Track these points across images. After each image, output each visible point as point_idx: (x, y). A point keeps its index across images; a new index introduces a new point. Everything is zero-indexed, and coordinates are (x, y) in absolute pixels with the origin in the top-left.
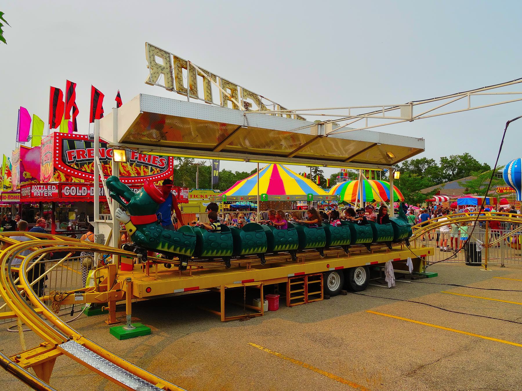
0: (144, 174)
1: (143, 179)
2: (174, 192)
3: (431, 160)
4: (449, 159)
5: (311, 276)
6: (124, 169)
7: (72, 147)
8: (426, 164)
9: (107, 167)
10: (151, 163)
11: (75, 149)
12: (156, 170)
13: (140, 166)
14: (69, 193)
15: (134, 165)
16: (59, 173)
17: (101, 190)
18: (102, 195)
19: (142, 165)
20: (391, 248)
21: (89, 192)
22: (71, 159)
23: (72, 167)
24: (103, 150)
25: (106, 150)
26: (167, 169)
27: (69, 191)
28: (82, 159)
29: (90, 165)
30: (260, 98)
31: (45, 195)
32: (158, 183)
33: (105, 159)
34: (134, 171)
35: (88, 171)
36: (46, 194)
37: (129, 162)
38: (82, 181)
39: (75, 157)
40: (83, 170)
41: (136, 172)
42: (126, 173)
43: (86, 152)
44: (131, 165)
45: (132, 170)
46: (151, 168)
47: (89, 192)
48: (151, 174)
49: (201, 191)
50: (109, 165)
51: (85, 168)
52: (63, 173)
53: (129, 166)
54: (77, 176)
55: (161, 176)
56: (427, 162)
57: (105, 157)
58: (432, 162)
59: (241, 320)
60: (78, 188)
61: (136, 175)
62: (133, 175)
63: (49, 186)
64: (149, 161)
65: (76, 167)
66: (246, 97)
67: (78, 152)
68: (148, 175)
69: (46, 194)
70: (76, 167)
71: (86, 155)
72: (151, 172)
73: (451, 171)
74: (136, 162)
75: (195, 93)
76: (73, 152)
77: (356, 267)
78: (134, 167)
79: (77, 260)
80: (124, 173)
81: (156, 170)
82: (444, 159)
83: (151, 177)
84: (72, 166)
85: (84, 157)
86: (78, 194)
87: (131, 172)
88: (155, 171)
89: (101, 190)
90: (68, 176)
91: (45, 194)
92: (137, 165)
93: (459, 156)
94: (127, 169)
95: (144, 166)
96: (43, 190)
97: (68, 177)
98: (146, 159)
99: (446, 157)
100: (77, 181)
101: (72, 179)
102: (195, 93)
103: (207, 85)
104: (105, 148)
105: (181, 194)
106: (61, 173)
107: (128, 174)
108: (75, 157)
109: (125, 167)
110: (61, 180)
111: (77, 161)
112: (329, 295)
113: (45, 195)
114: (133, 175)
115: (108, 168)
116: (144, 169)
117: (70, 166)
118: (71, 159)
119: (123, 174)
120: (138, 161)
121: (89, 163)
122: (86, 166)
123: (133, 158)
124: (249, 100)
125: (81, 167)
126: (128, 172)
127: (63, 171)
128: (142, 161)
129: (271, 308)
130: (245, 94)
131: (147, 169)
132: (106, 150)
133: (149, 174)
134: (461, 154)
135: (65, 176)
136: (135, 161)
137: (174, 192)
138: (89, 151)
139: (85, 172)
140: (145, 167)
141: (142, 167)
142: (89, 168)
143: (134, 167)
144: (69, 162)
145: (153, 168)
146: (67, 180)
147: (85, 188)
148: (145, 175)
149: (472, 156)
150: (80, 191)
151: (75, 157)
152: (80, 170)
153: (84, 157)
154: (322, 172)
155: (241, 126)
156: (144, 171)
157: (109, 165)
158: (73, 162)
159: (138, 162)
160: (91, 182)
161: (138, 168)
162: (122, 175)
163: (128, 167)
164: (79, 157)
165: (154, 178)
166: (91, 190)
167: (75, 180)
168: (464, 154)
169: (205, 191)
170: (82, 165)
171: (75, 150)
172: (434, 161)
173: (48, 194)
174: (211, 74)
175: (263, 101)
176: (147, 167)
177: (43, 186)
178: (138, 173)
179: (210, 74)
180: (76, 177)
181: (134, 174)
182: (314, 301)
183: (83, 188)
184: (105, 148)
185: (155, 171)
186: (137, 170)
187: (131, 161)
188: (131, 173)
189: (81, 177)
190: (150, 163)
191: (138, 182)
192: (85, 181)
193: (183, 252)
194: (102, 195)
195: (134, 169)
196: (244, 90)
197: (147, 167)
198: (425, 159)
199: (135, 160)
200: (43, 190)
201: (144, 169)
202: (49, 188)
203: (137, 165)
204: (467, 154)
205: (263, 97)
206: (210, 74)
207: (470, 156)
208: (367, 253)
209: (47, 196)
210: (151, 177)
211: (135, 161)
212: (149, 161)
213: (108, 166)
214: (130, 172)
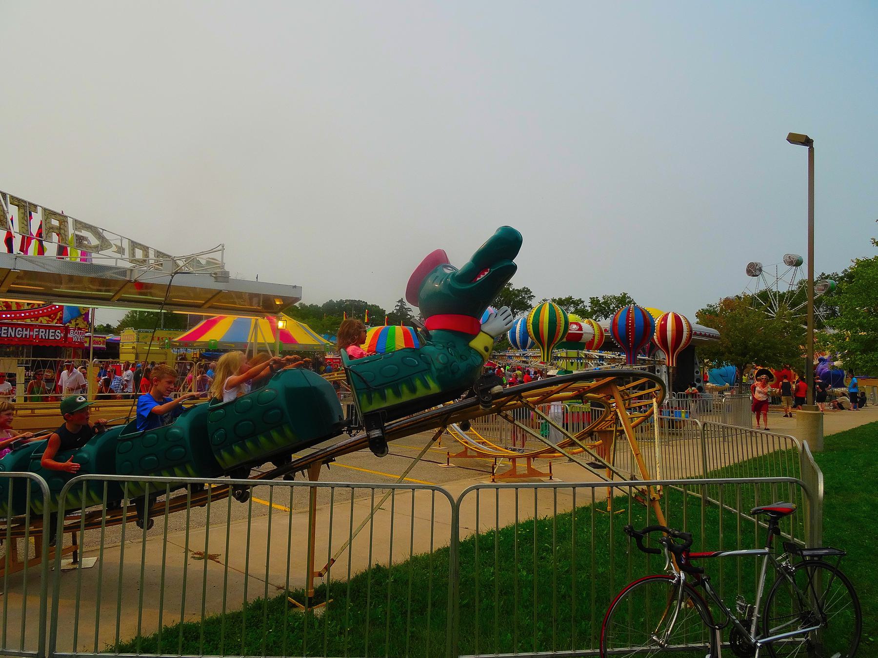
2: (58, 332)
3: (578, 301)
4: (602, 301)
8: (572, 305)
14: (21, 335)
17: (46, 333)
18: (47, 338)
30: (101, 231)
32: (39, 320)
49: (170, 332)
55: (47, 310)
56: (573, 302)
58: (580, 303)
61: (5, 309)
68: (22, 308)
73: (603, 318)
75: (5, 224)
82: (594, 300)
89: (46, 333)
93: (615, 298)
99: (597, 298)
102: (5, 224)
103: (23, 215)
105: (69, 336)
124: (84, 233)
130: (79, 226)
134: (618, 295)
149: (632, 298)
154: (411, 311)
155: (11, 269)
165: (45, 311)
168: (621, 294)
169: (176, 332)
172: (583, 302)
174: (29, 203)
175: (105, 234)
179: (27, 204)
191: (6, 318)
194: (47, 338)
196: (76, 222)
198: (571, 298)
204: (625, 294)
206: (27, 204)
207: (629, 297)
210: (27, 312)
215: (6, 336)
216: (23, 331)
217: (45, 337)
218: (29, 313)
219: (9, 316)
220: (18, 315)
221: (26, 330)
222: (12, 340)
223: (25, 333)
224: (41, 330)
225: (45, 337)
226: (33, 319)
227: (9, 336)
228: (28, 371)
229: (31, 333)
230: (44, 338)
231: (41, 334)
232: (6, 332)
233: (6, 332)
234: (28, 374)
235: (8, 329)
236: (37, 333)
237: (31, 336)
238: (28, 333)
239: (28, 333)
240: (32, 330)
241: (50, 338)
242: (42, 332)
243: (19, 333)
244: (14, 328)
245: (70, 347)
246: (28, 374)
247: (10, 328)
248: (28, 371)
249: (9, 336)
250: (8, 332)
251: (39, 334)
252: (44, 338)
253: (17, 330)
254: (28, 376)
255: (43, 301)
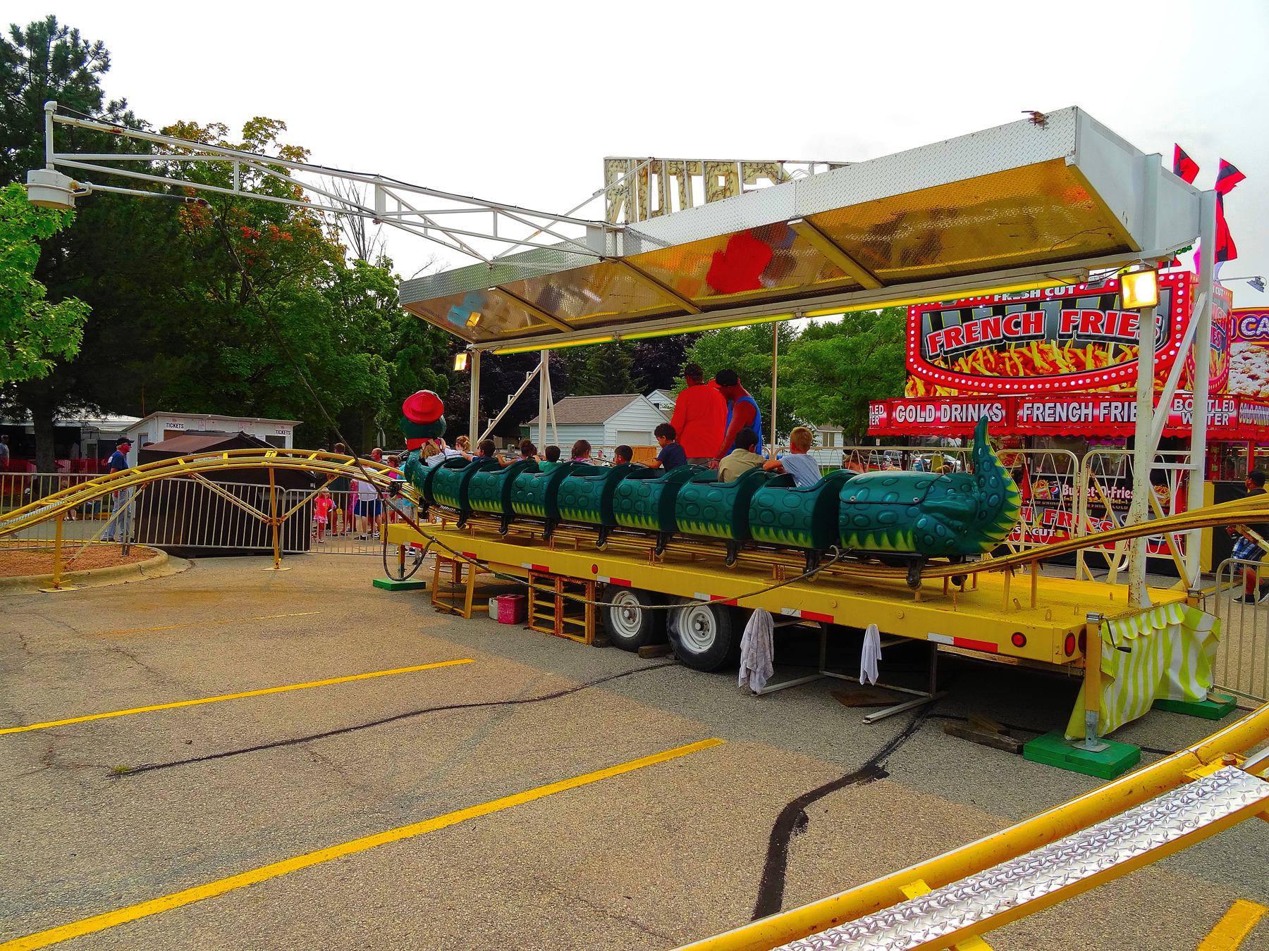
0: (1096, 364)
1: (1092, 377)
2: (997, 408)
5: (579, 583)
6: (1042, 357)
7: (937, 324)
9: (1004, 358)
10: (1116, 334)
11: (942, 328)
12: (1131, 349)
13: (1083, 347)
15: (1068, 345)
16: (913, 379)
17: (1123, 409)
18: (1126, 420)
19: (1090, 343)
20: (914, 584)
21: (938, 414)
22: (934, 349)
23: (937, 367)
24: (996, 321)
25: (1003, 319)
26: (1167, 342)
27: (904, 414)
28: (955, 346)
29: (970, 358)
31: (1216, 423)
33: (1001, 341)
34: (1068, 359)
35: (966, 370)
36: (1218, 421)
37: (1055, 339)
38: (955, 392)
39: (942, 346)
40: (957, 369)
41: (1073, 361)
42: (1046, 366)
43: (963, 331)
44: (1061, 346)
45: (1064, 358)
46: (1116, 346)
47: (938, 414)
48: (1114, 364)
50: (1009, 352)
51: (960, 366)
52: (921, 379)
53: (1056, 350)
54: (944, 384)
57: (1002, 337)
59: (949, 732)
60: (919, 407)
61: (1074, 369)
62: (1064, 370)
63: (1225, 401)
64: (1110, 330)
65: (943, 365)
66: (750, 179)
67: (947, 334)
68: (1105, 365)
69: (1218, 421)
70: (943, 365)
71: (1102, 325)
72: (1115, 356)
74: (1075, 336)
76: (939, 334)
77: (681, 597)
78: (1069, 351)
79: (1073, 564)
80: (1042, 368)
81: (1131, 349)
83: (1113, 371)
84: (936, 363)
85: (958, 342)
86: (919, 420)
87: (1060, 362)
88: (1126, 354)
89: (1123, 409)
90: (929, 384)
91: (1217, 419)
92: (1076, 345)
94: (1051, 358)
95: (1094, 344)
96: (1213, 411)
97: (928, 387)
98: (1102, 325)
100: (945, 394)
101: (936, 391)
104: (1001, 317)
106: (917, 380)
107: (1051, 369)
108: (943, 344)
109: (1047, 353)
110: (917, 393)
111: (946, 353)
112: (605, 636)
113: (1216, 423)
114: (1064, 370)
115: (1007, 360)
116: (1094, 351)
117: (932, 365)
118: (934, 349)
119: (1041, 371)
120: (1079, 333)
121: (968, 354)
122: (961, 360)
123: (1066, 328)
125: (953, 364)
126: (1053, 364)
127: (920, 376)
128: (1090, 332)
129: (503, 620)
131: (1103, 350)
132: (1003, 319)
133: (1110, 364)
135: (925, 385)
136: (1070, 336)
137: (997, 408)
138: (968, 328)
139: (961, 373)
140: (1097, 347)
141: (1090, 348)
142: (967, 364)
143: (1069, 351)
144: (931, 358)
145: (1122, 346)
146: (928, 391)
147: (932, 407)
148: (1097, 366)
150: (923, 414)
151: (943, 344)
152: (950, 371)
153: (958, 342)
156: (1096, 358)
157: (1009, 352)
158: (938, 356)
159: (1079, 336)
160: (970, 393)
161: (1079, 352)
162: (1038, 373)
163: (1052, 353)
164: (950, 345)
166: (943, 410)
167: (941, 391)
170: (955, 359)
171: (942, 332)
173: (1221, 421)
176: (1103, 347)
177: (1213, 401)
178: (1080, 364)
180: (942, 386)
181: (1068, 367)
182: (569, 638)
183: (928, 407)
184: (1001, 317)
185: (1126, 354)
186: (1075, 355)
187: (1061, 336)
188: (1060, 366)
189: (952, 385)
190: (1113, 335)
191: (1077, 387)
192: (960, 393)
193: (886, 545)
194: (1126, 420)
195: (1068, 355)
197: (1103, 347)
199: (1071, 332)
200: (1213, 411)
201: (1096, 353)
202: (1225, 405)
203: (1076, 345)
205: (784, 162)
208: (803, 581)
209: (1220, 424)
210: (1113, 371)
211: (1070, 336)
212: (1110, 330)
213: (1006, 354)
214: (1057, 362)
215: (1052, 419)
216: (1080, 408)
217: (1123, 418)
218: (1117, 372)
219: (1080, 382)
220: (1097, 379)
221: (1086, 407)
222: (1101, 427)
223: (1084, 411)
224: (1114, 404)
225: (1123, 418)
226: (1124, 385)
227: (1057, 420)
228: (1121, 489)
229: (1096, 412)
230: (959, 420)
231: (1036, 412)
232: (1052, 412)
233: (1052, 412)
234: (1121, 494)
235: (1055, 407)
236: (1106, 412)
237: (1095, 418)
238: (1089, 411)
239: (1089, 411)
240: (1096, 406)
241: (1047, 419)
242: (1116, 408)
243: (1075, 412)
244: (1065, 404)
245: (1046, 436)
246: (1121, 494)
247: (1058, 404)
248: (1121, 489)
249: (1057, 420)
250: (1055, 413)
251: (1032, 412)
252: (1120, 420)
253: (948, 417)
254: (1120, 498)
255: (608, 336)
